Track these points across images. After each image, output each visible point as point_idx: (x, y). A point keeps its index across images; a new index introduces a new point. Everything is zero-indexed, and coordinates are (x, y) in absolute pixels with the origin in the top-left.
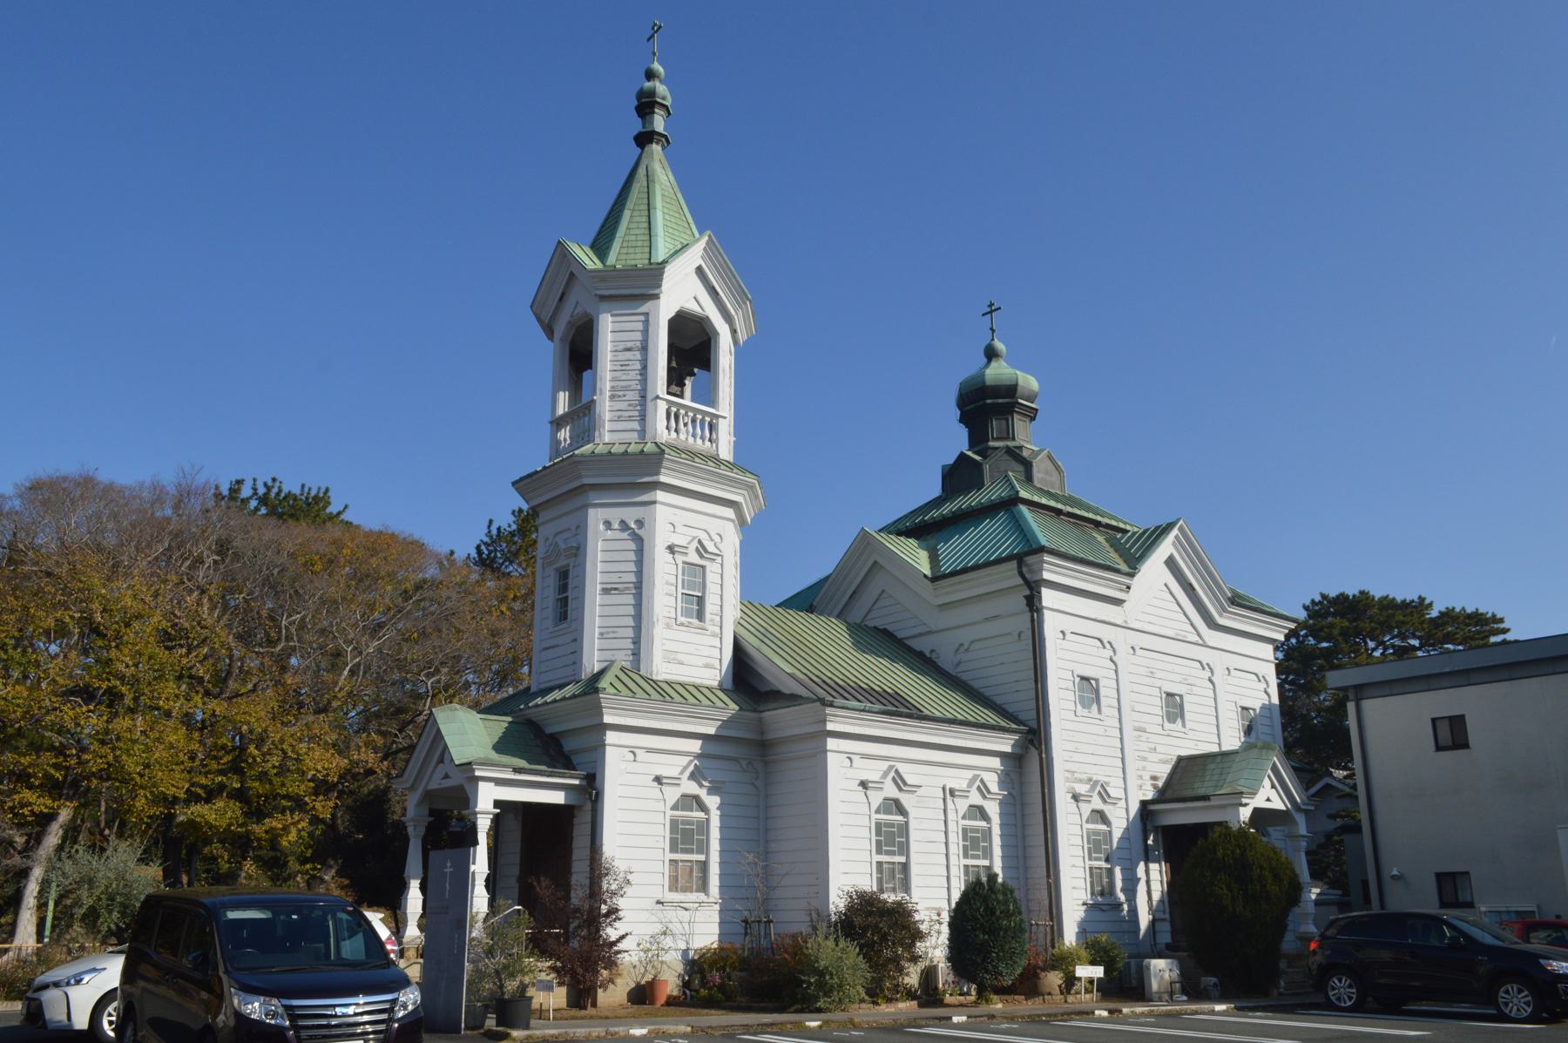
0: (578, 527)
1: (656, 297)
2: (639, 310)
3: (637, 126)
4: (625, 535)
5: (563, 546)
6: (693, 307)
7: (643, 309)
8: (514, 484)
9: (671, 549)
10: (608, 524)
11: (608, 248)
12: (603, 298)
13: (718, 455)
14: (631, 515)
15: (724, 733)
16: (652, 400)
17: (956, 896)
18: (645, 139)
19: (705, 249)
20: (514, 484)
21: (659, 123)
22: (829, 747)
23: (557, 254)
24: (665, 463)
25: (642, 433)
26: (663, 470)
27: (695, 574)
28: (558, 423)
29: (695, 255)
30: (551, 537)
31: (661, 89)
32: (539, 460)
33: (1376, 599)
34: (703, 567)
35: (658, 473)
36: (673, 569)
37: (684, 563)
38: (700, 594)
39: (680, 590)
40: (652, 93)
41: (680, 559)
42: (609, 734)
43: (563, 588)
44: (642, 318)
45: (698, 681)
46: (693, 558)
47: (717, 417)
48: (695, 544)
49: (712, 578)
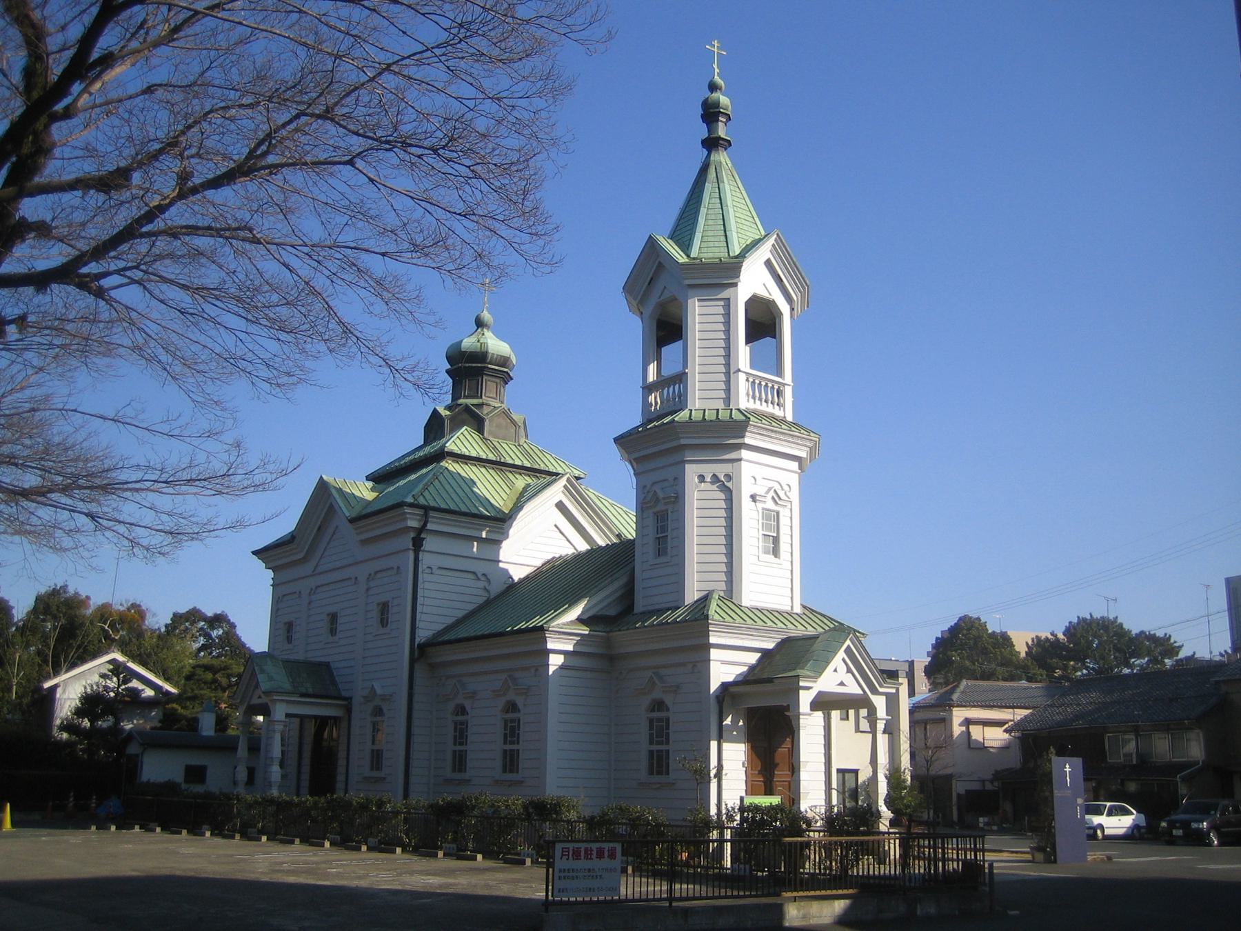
0: (675, 479)
1: (735, 285)
2: (719, 296)
3: (703, 132)
4: (714, 487)
5: (661, 495)
6: (763, 293)
7: (724, 294)
8: (616, 440)
9: (753, 498)
10: (702, 478)
11: (691, 240)
12: (691, 286)
13: (785, 417)
14: (721, 470)
15: (579, 649)
16: (734, 373)
17: (941, 773)
18: (712, 143)
19: (773, 245)
20: (616, 440)
21: (722, 131)
22: (712, 657)
23: (648, 245)
24: (749, 429)
25: (727, 400)
26: (747, 434)
27: (772, 519)
28: (648, 389)
29: (765, 252)
30: (649, 486)
31: (724, 100)
32: (634, 419)
33: (1230, 651)
34: (778, 513)
35: (743, 437)
36: (755, 515)
37: (763, 509)
38: (775, 535)
39: (761, 532)
40: (717, 104)
41: (760, 505)
42: (551, 656)
43: (663, 529)
44: (722, 303)
45: (760, 605)
46: (770, 505)
47: (784, 385)
48: (772, 493)
49: (784, 521)
